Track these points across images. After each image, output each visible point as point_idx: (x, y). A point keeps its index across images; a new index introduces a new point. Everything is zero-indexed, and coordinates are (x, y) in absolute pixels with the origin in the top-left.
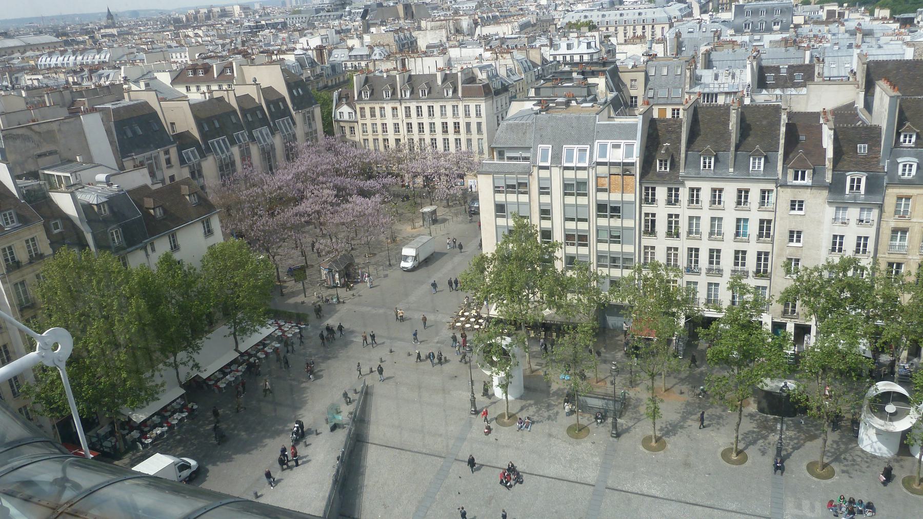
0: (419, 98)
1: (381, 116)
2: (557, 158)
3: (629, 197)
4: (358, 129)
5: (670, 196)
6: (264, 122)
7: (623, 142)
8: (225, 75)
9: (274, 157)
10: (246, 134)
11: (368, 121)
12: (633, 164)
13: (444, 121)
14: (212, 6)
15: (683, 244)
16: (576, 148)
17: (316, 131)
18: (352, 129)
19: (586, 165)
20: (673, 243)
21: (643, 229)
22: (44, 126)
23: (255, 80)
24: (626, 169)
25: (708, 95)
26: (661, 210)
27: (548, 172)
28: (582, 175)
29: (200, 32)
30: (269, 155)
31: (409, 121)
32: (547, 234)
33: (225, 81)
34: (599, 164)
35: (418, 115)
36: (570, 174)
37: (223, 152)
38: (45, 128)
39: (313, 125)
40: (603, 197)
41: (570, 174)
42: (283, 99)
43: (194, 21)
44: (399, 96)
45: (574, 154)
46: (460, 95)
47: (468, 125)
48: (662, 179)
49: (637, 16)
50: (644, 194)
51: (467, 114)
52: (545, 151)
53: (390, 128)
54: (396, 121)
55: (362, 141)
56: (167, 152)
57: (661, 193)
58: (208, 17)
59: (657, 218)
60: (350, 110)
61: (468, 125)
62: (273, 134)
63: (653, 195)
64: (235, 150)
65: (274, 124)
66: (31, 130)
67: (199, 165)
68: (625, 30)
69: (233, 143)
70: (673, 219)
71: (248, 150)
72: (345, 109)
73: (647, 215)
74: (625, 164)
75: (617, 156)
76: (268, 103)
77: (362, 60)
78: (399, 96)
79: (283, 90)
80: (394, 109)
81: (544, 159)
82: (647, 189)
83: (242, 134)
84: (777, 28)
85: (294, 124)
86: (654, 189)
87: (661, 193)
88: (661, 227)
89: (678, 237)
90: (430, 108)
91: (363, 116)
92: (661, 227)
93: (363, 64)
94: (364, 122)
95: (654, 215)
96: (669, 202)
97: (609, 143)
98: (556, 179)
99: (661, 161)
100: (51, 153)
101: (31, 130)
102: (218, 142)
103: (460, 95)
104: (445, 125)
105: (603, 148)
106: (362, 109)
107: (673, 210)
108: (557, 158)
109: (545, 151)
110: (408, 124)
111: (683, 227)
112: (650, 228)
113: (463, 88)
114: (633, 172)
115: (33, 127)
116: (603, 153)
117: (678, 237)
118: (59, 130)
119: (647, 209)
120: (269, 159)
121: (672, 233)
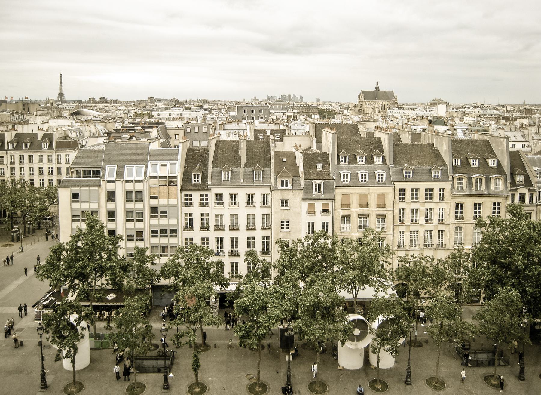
2: (120, 174)
3: (173, 202)
7: (168, 162)
12: (175, 178)
13: (41, 166)
16: (135, 167)
19: (142, 178)
24: (171, 181)
26: (196, 211)
28: (139, 187)
31: (13, 166)
34: (151, 178)
40: (154, 202)
45: (134, 171)
46: (54, 147)
47: (59, 169)
48: (196, 187)
57: (196, 197)
59: (194, 217)
73: (186, 214)
74: (170, 178)
78: (6, 148)
81: (111, 175)
82: (186, 195)
87: (196, 197)
88: (197, 223)
89: (208, 230)
90: (31, 156)
95: (191, 214)
97: (159, 162)
98: (120, 189)
103: (54, 147)
107: (205, 210)
108: (120, 174)
112: (190, 225)
117: (208, 230)
119: (187, 210)
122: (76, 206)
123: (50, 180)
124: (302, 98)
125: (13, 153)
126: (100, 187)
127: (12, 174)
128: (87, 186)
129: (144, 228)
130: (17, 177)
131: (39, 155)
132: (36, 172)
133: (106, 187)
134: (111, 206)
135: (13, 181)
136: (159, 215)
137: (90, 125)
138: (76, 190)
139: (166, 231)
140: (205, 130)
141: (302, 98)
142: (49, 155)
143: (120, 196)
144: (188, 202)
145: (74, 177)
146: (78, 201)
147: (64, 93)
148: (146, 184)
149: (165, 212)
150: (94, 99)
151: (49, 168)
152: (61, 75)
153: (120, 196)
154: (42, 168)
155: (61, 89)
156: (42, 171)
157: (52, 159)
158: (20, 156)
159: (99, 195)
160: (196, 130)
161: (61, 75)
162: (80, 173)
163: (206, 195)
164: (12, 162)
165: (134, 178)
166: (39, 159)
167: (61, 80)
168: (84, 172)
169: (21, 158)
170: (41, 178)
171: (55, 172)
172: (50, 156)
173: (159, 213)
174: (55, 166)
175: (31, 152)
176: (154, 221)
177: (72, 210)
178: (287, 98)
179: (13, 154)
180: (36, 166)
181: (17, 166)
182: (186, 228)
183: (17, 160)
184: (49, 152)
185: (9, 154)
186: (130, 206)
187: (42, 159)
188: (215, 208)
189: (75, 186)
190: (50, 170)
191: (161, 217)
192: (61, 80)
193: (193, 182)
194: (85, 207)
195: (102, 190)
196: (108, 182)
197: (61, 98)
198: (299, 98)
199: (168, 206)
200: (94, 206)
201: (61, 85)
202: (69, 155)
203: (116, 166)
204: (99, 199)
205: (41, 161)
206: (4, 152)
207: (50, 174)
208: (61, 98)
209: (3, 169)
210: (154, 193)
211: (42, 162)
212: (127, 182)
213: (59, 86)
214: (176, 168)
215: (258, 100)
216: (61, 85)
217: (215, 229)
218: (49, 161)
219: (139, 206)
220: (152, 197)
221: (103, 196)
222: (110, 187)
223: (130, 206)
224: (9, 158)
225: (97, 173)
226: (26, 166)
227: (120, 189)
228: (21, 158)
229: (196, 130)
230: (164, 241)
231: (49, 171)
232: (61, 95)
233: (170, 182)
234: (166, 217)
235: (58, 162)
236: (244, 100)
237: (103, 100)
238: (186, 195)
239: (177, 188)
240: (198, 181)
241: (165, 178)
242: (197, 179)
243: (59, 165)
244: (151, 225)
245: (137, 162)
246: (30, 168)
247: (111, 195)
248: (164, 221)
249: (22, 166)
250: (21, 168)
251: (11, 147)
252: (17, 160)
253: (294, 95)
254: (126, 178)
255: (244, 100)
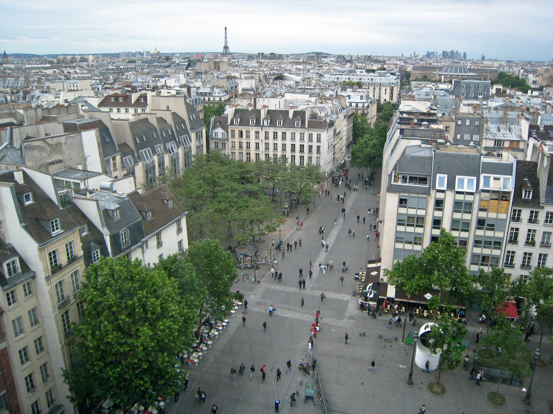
0: (276, 126)
1: (247, 137)
2: (451, 185)
3: (502, 216)
4: (229, 145)
5: (531, 216)
6: (172, 138)
7: (502, 177)
8: (142, 102)
9: (178, 163)
10: (162, 146)
11: (237, 140)
12: (509, 193)
13: (293, 143)
14: (74, 55)
15: (536, 251)
16: (466, 178)
17: (202, 145)
18: (224, 145)
19: (474, 190)
20: (529, 249)
21: (508, 239)
22: (55, 139)
23: (168, 107)
24: (503, 196)
25: (498, 140)
26: (524, 227)
27: (472, 196)
28: (469, 198)
29: (78, 71)
30: (175, 162)
31: (267, 141)
32: (434, 239)
33: (139, 107)
34: (483, 191)
35: (274, 138)
36: (460, 197)
37: (148, 158)
38: (55, 140)
39: (201, 141)
40: (483, 215)
41: (460, 197)
42: (184, 122)
43: (291, 55)
44: (262, 124)
45: (466, 183)
46: (306, 126)
47: (310, 147)
48: (526, 203)
49: (370, 81)
50: (512, 214)
51: (310, 140)
52: (442, 179)
53: (253, 146)
54: (257, 141)
55: (230, 153)
56: (114, 159)
57: (525, 214)
58: (72, 62)
59: (520, 232)
60: (223, 132)
61: (310, 147)
62: (178, 147)
63: (519, 215)
64: (156, 158)
65: (179, 139)
66: (46, 142)
67: (133, 168)
68: (380, 89)
69: (154, 152)
70: (531, 233)
71: (163, 158)
72: (220, 131)
73: (512, 229)
74: (503, 192)
75: (494, 185)
76: (175, 124)
77: (206, 96)
78: (262, 124)
79: (183, 114)
80: (257, 133)
81: (441, 184)
82: (515, 211)
83: (160, 147)
84: (480, 97)
85: (190, 140)
86: (520, 211)
87: (525, 214)
88: (522, 238)
89: (533, 246)
90: (284, 134)
91: (233, 136)
92: (522, 238)
93: (207, 98)
94: (233, 140)
95: (517, 229)
96: (530, 221)
97: (492, 176)
98: (449, 199)
99: (526, 191)
100: (59, 161)
101: (46, 142)
102: (145, 152)
103: (306, 126)
104: (293, 146)
105: (487, 179)
106: (233, 131)
107: (533, 227)
108: (451, 185)
109: (442, 179)
110: (266, 143)
111: (538, 239)
112: (514, 240)
113: (308, 121)
114: (508, 199)
115: (47, 140)
116: (487, 183)
117: (533, 246)
118: (65, 143)
119: (514, 225)
120: (175, 165)
121: (530, 242)
122: (403, 211)
123: (301, 157)
124: (465, 54)
125: (267, 129)
126: (430, 195)
127: (266, 149)
128: (417, 193)
129: (468, 238)
130: (279, 154)
131: (292, 133)
132: (289, 148)
133: (434, 196)
134: (438, 214)
135: (267, 155)
136: (485, 226)
137: (327, 101)
138: (404, 195)
139: (490, 243)
140: (477, 123)
141: (465, 54)
142: (301, 134)
143: (448, 205)
144: (516, 218)
145: (400, 183)
146: (405, 207)
147: (229, 45)
148: (477, 196)
149: (493, 225)
150: (263, 54)
151: (301, 145)
152: (226, 29)
153: (448, 205)
154: (294, 145)
155: (226, 42)
156: (294, 148)
157: (303, 137)
158: (274, 132)
159: (427, 203)
160: (468, 123)
161: (226, 29)
162: (406, 179)
163: (537, 213)
164: (267, 138)
165: (465, 189)
166: (292, 136)
167: (226, 33)
168: (410, 178)
169: (275, 134)
170: (293, 154)
171: (306, 149)
172: (302, 135)
173: (486, 224)
174: (306, 145)
175: (284, 130)
176: (480, 233)
177: (398, 214)
178: (449, 54)
179: (267, 130)
180: (288, 143)
181: (271, 141)
182: (510, 241)
183: (271, 136)
184: (302, 131)
185: (264, 130)
186: (458, 216)
187: (294, 136)
188: (544, 226)
189: (404, 192)
190: (302, 147)
191: (488, 229)
192: (226, 33)
193: (523, 197)
194: (412, 212)
195: (431, 198)
196: (438, 191)
197: (226, 51)
198: (462, 55)
199: (497, 219)
200: (421, 213)
201: (226, 38)
202: (320, 135)
203: (446, 176)
204: (427, 206)
205: (293, 138)
206: (260, 128)
207: (302, 151)
208: (226, 51)
209: (258, 143)
210: (484, 206)
211: (294, 139)
212: (458, 193)
213: (224, 39)
214: (508, 183)
215: (418, 56)
216: (226, 38)
217: (541, 246)
218: (301, 139)
219: (467, 217)
220: (481, 210)
221: (431, 204)
222: (440, 196)
223: (458, 216)
224: (264, 134)
225: (423, 180)
226: (280, 142)
227: (449, 199)
228: (275, 134)
229: (468, 123)
230: (487, 252)
231: (301, 148)
232: (226, 48)
233: (503, 197)
234: (493, 230)
235: (309, 140)
236: (403, 55)
237: (273, 56)
238: (515, 211)
239: (509, 203)
240: (528, 197)
241: (498, 192)
242: (527, 195)
243: (310, 144)
244: (475, 236)
245: (467, 174)
246: (283, 144)
247: (439, 204)
248: (490, 233)
249: (276, 142)
250: (274, 144)
251: (265, 124)
252: (271, 136)
253: (457, 51)
254: (457, 189)
255: (403, 55)
